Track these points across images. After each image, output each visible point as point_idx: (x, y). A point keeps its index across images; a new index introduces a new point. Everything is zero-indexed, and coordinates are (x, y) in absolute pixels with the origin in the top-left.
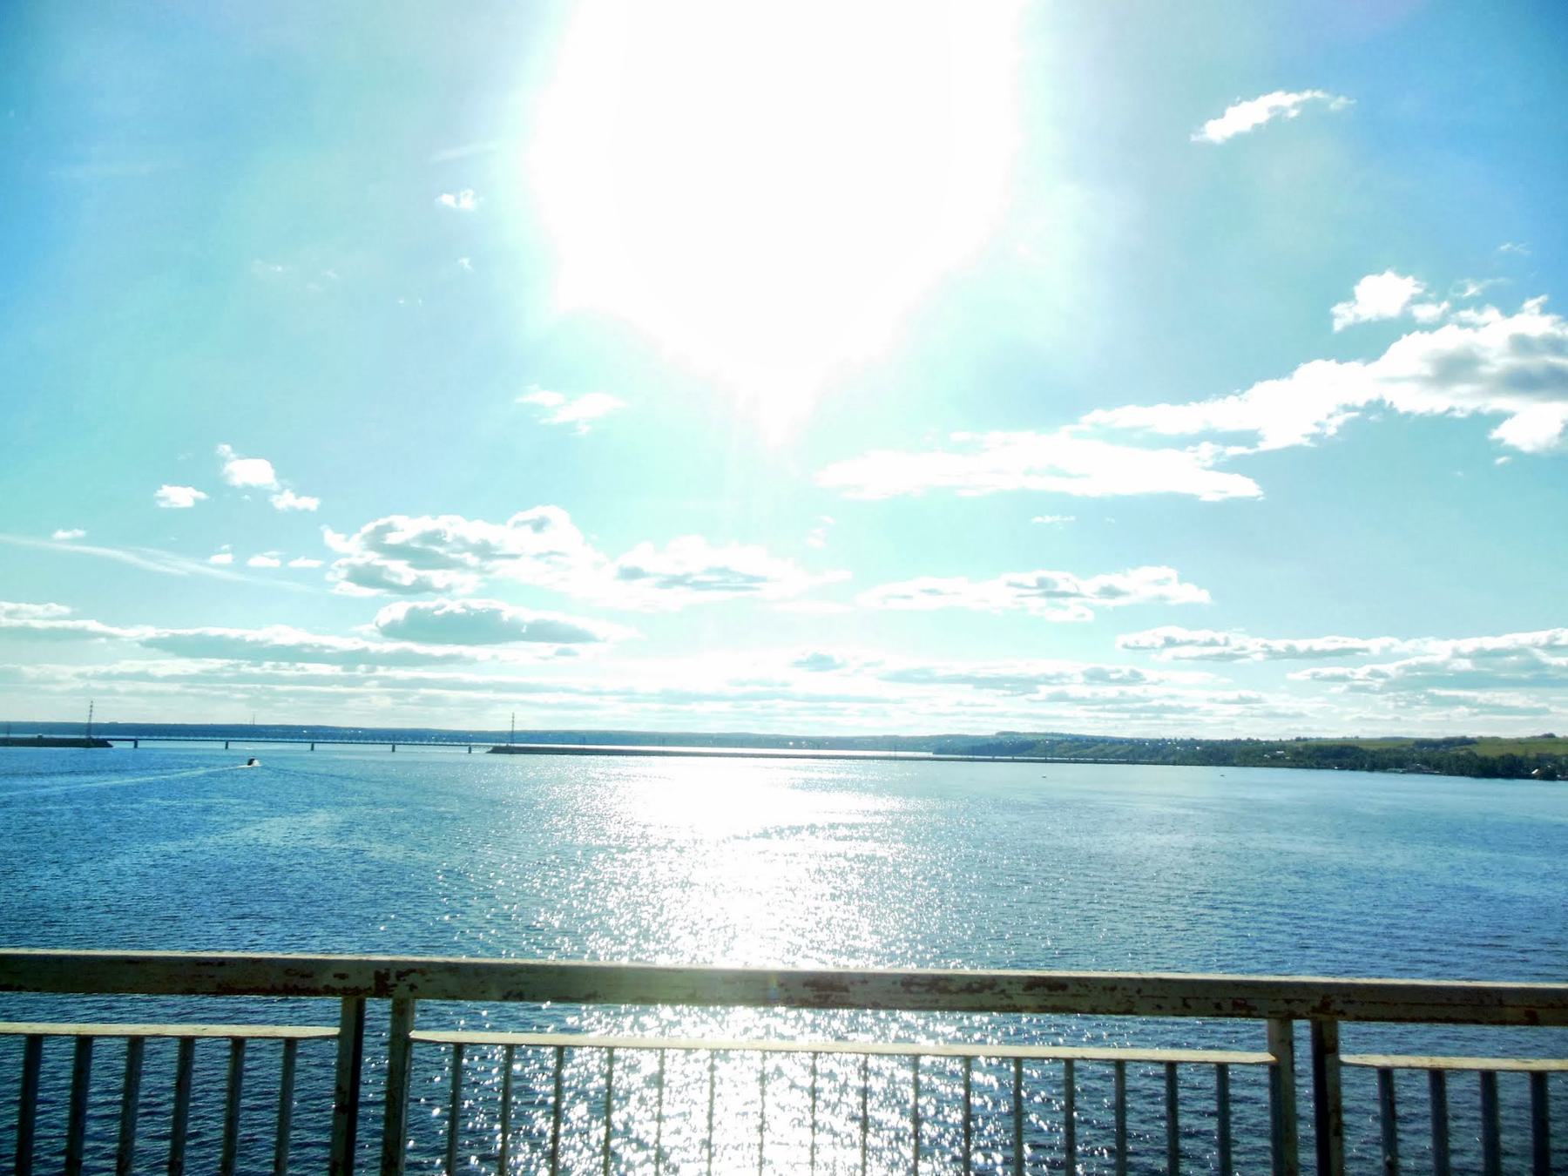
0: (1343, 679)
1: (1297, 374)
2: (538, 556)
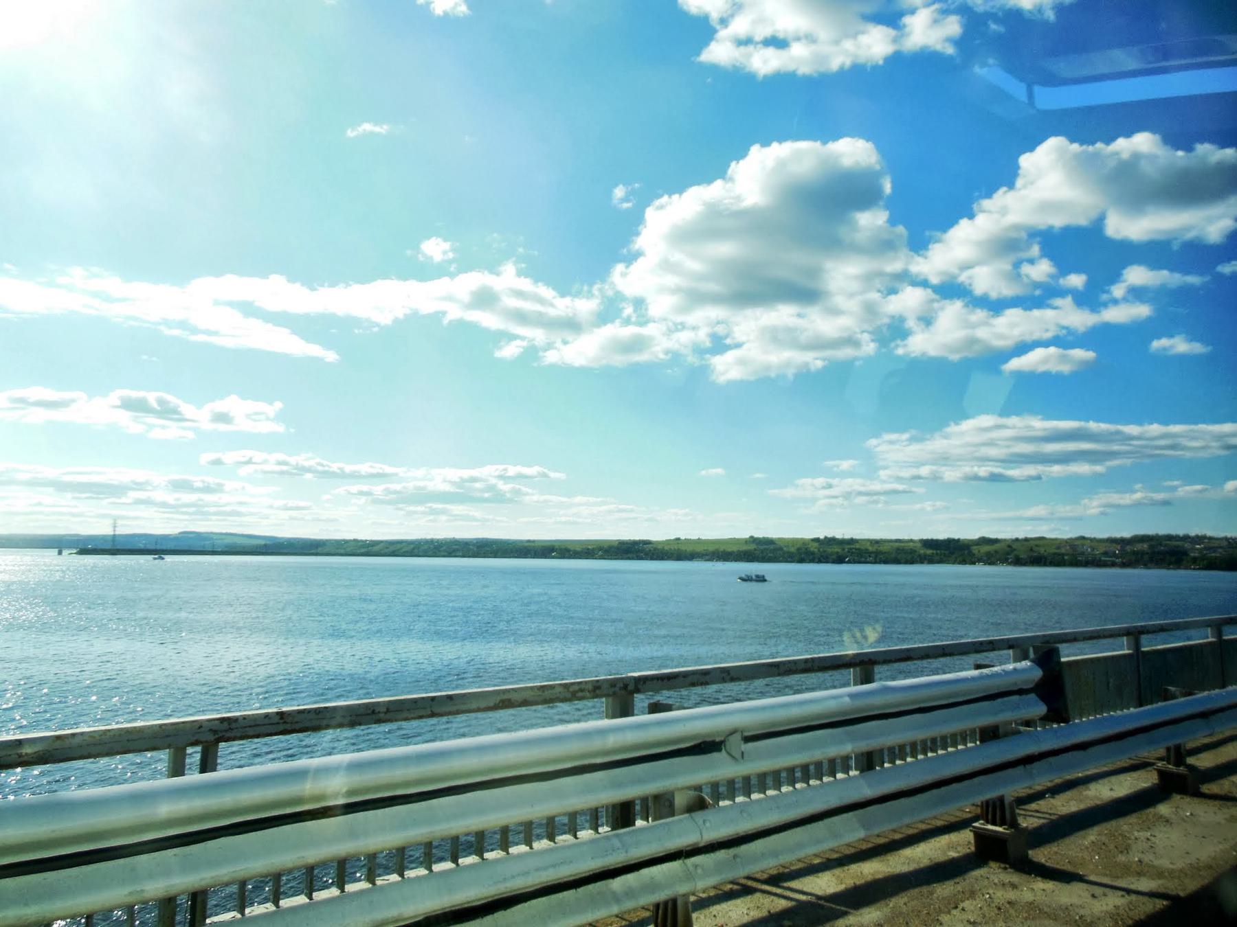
0: (368, 494)
1: (408, 282)
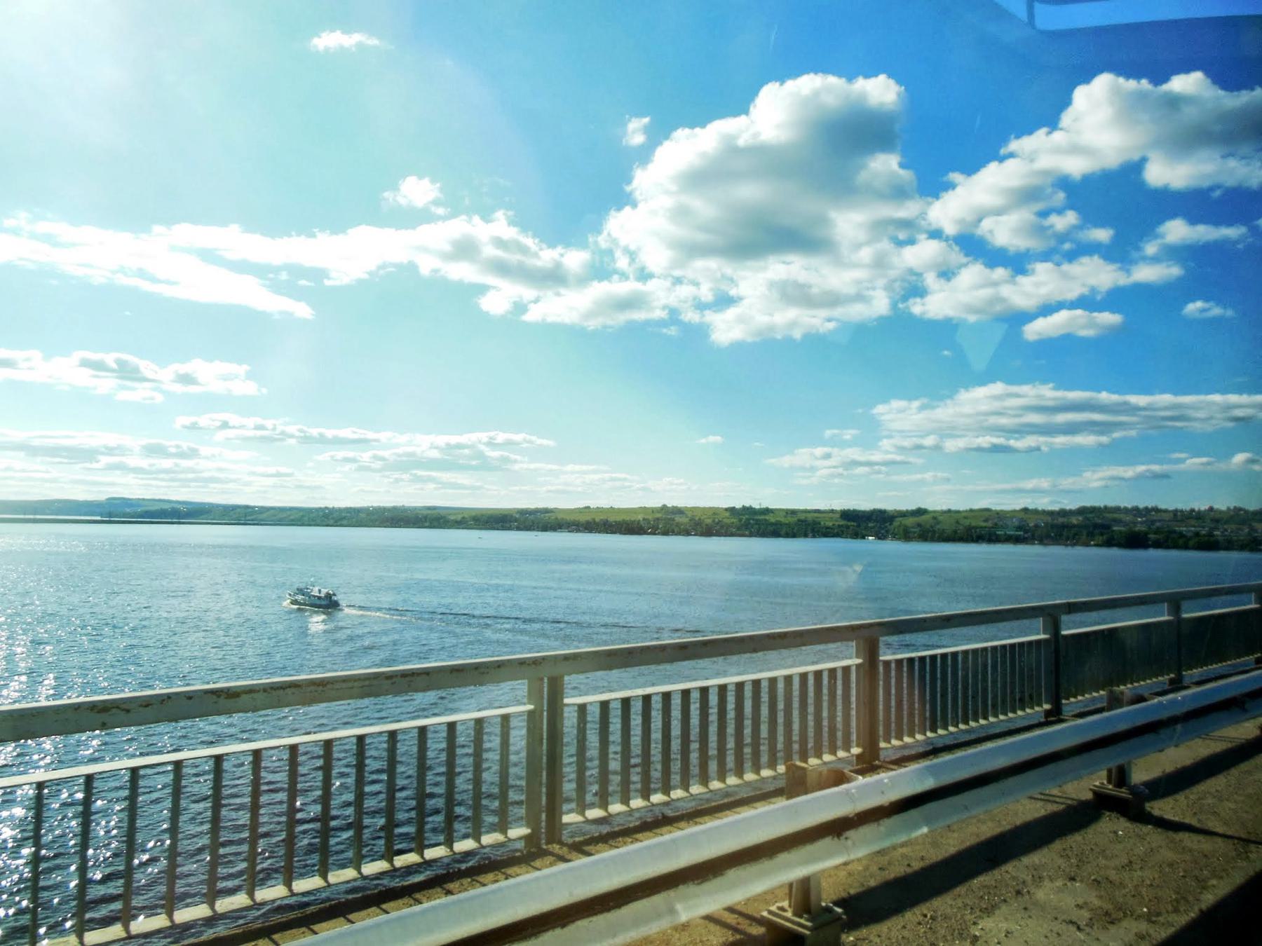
0: (354, 460)
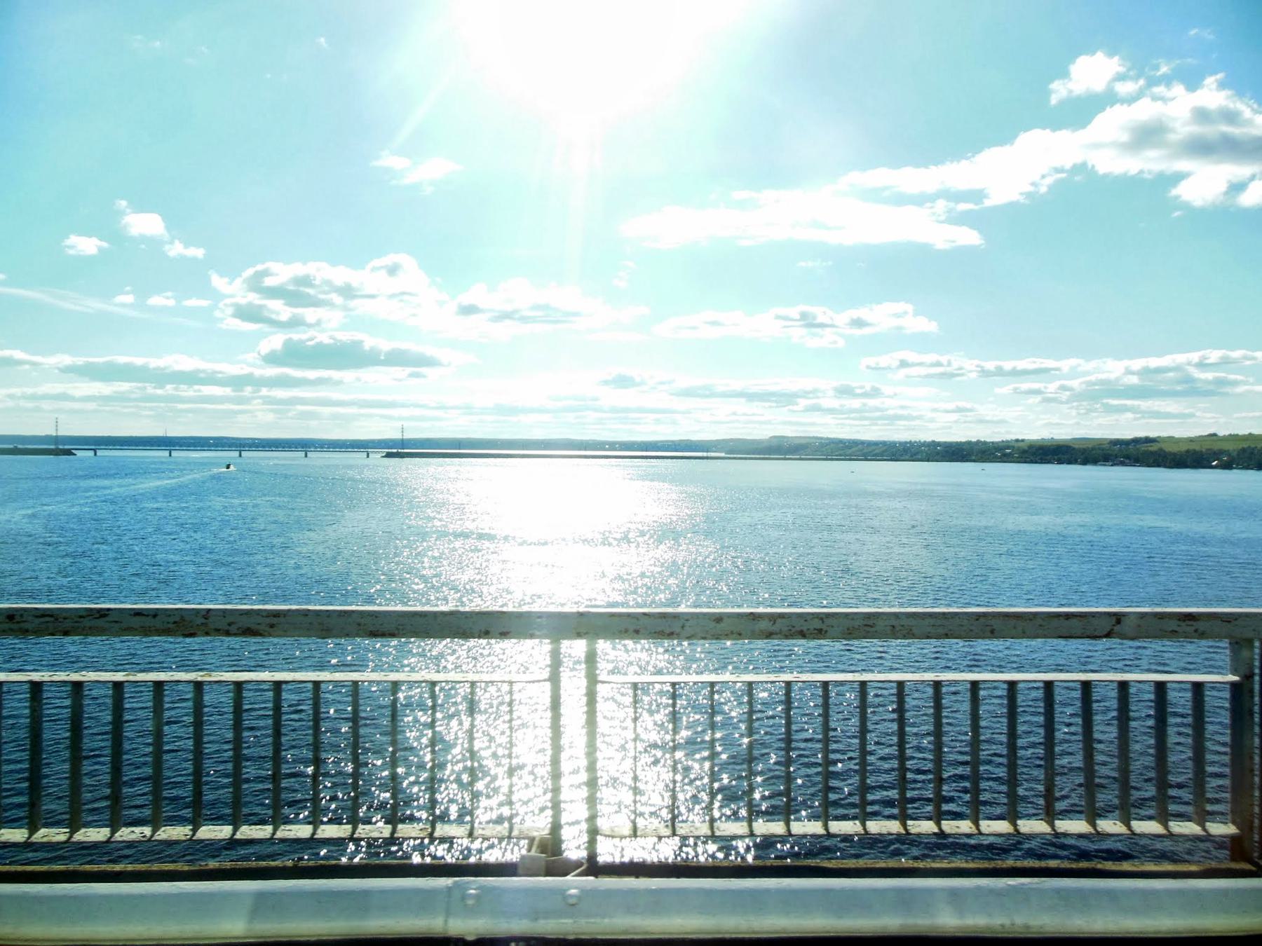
0: (1038, 392)
2: (393, 296)
